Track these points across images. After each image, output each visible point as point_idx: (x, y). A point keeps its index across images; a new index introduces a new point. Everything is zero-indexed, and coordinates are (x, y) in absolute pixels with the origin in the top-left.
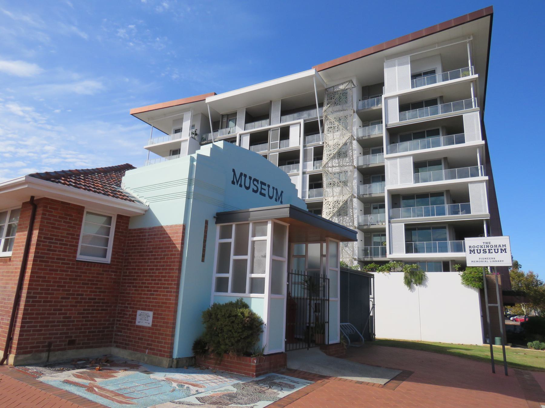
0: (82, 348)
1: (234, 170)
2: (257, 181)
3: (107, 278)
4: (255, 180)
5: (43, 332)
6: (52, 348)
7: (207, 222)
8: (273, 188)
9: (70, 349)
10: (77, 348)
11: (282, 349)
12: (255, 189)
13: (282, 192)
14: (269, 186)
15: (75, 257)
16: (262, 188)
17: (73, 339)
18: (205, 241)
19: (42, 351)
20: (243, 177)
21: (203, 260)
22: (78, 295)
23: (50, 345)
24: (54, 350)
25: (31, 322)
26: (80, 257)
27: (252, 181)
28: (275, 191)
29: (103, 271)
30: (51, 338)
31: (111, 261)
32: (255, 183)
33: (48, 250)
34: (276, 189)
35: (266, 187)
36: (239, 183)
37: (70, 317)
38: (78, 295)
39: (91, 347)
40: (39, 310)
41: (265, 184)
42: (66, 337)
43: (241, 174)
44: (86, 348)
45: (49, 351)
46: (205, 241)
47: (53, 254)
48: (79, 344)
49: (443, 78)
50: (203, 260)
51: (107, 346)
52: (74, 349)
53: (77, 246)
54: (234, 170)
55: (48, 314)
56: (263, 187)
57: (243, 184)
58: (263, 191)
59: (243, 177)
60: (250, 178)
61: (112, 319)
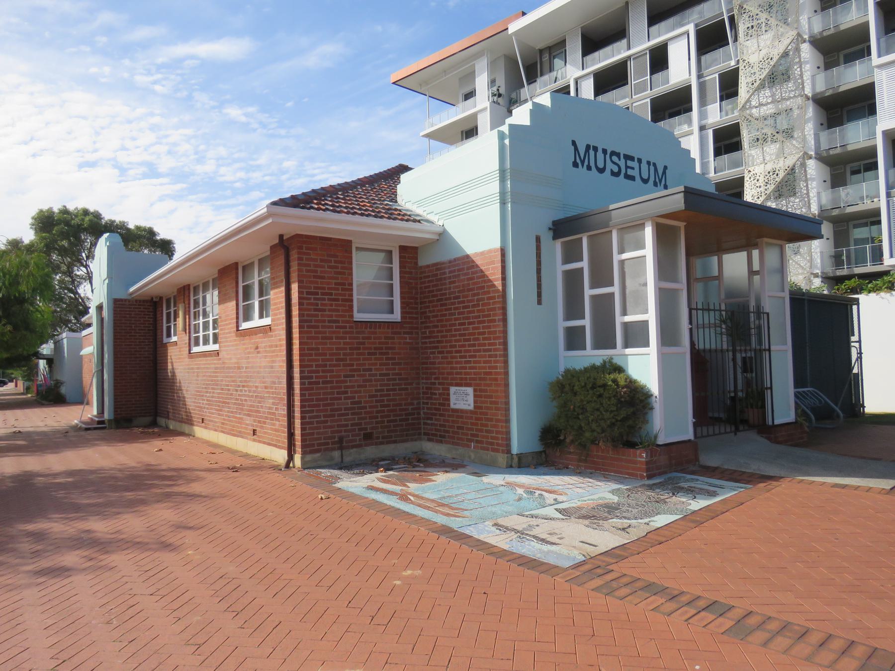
0: (382, 443)
1: (574, 143)
2: (618, 155)
3: (400, 343)
4: (613, 153)
5: (329, 424)
6: (344, 444)
7: (538, 239)
8: (649, 163)
9: (366, 445)
10: (376, 444)
12: (616, 169)
13: (665, 168)
14: (640, 161)
15: (352, 316)
16: (627, 167)
17: (369, 431)
18: (539, 271)
19: (333, 449)
20: (592, 152)
21: (539, 302)
22: (364, 370)
23: (341, 440)
24: (348, 448)
25: (312, 411)
26: (358, 316)
27: (608, 156)
28: (652, 168)
29: (392, 333)
30: (341, 431)
31: (402, 318)
32: (615, 158)
33: (315, 310)
34: (654, 164)
35: (635, 164)
36: (586, 163)
37: (360, 402)
40: (319, 394)
41: (632, 158)
42: (360, 430)
43: (588, 147)
44: (388, 443)
45: (341, 448)
46: (539, 271)
47: (322, 316)
48: (378, 438)
49: (121, 300)
50: (539, 302)
52: (372, 444)
54: (574, 143)
55: (331, 399)
56: (630, 163)
57: (592, 164)
58: (630, 172)
59: (592, 152)
60: (605, 151)
61: (415, 402)
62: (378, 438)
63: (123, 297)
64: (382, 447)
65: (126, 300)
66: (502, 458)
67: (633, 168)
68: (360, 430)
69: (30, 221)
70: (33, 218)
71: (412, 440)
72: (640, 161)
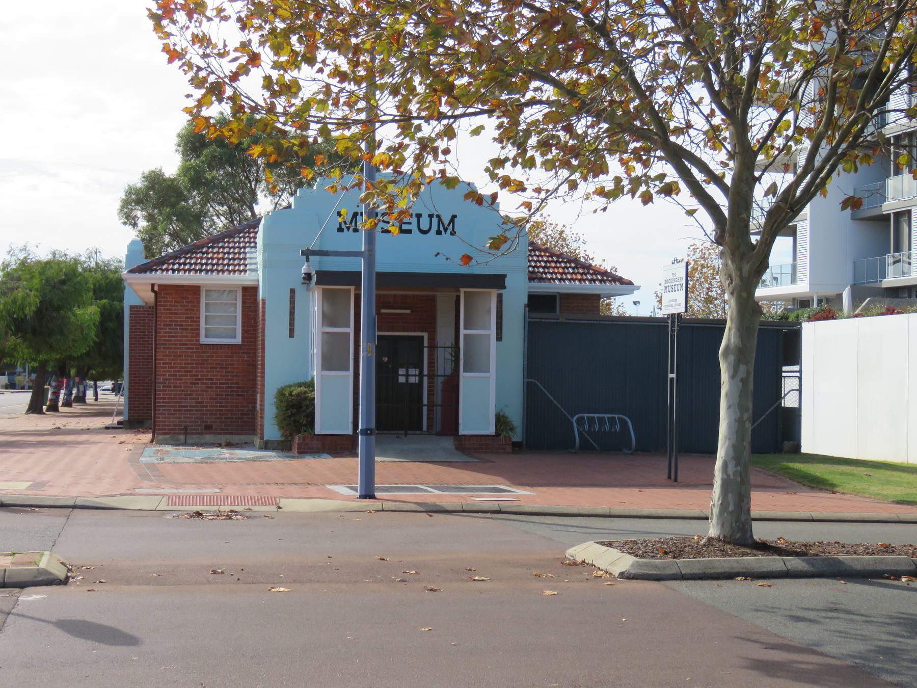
0: (220, 434)
7: (293, 291)
8: (431, 216)
10: (215, 433)
11: (462, 431)
15: (198, 341)
18: (292, 314)
21: (291, 334)
22: (207, 380)
23: (186, 428)
24: (192, 434)
26: (203, 340)
28: (435, 220)
34: (438, 216)
35: (414, 220)
38: (207, 380)
39: (231, 434)
42: (202, 422)
44: (225, 434)
45: (186, 434)
46: (292, 314)
48: (216, 429)
49: (136, 307)
50: (291, 334)
51: (250, 434)
53: (199, 329)
58: (405, 227)
61: (250, 405)
62: (216, 429)
63: (137, 304)
64: (220, 436)
65: (140, 307)
66: (257, 441)
67: (410, 223)
68: (202, 422)
69: (176, 140)
70: (179, 136)
71: (246, 434)
72: (419, 216)
